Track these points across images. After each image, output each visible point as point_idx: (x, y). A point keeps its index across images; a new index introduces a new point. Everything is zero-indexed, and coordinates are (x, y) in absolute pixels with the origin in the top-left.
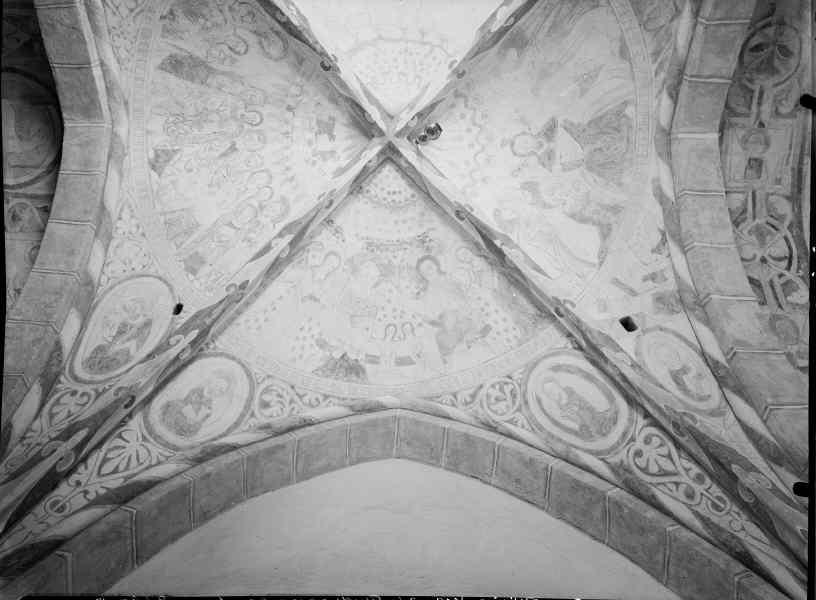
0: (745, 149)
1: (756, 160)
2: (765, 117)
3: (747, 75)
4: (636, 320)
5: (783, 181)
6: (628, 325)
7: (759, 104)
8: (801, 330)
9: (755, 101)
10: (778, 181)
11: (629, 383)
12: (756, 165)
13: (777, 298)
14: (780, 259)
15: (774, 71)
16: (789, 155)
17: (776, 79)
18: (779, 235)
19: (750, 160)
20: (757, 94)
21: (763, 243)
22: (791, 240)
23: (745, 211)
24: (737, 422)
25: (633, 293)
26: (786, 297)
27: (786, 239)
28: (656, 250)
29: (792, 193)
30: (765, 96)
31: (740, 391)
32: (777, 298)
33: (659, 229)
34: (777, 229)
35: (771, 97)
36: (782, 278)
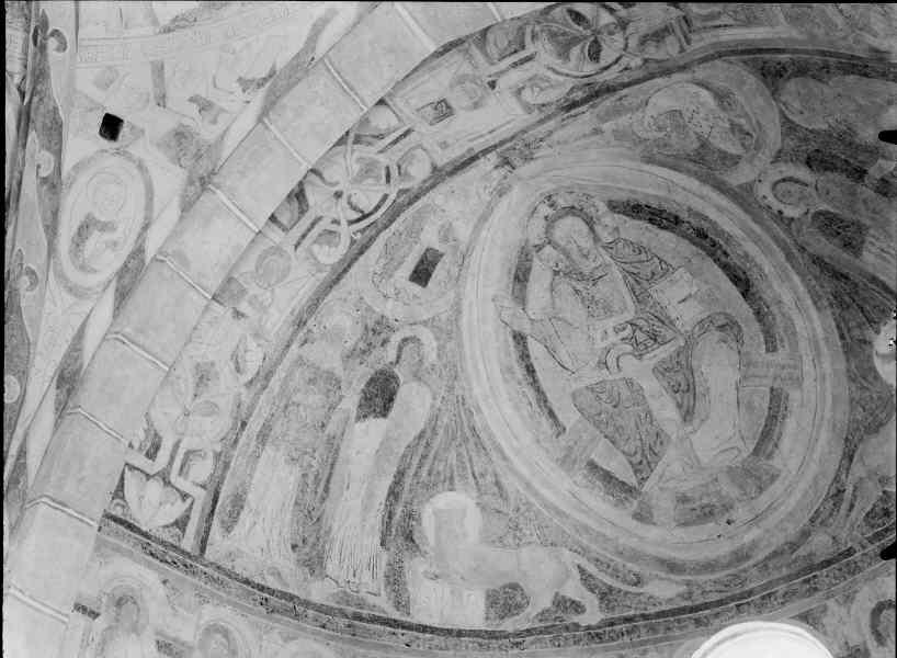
0: (451, 86)
1: (448, 107)
2: (502, 83)
3: (538, 28)
4: (124, 131)
5: (450, 149)
6: (111, 126)
7: (515, 65)
8: (288, 280)
9: (515, 58)
10: (444, 145)
11: (19, 190)
12: (443, 110)
13: (304, 236)
14: (355, 208)
15: (564, 53)
16: (482, 136)
17: (557, 63)
18: (384, 188)
19: (444, 101)
20: (522, 55)
21: (358, 180)
22: (389, 202)
23: (380, 137)
24: (84, 316)
25: (162, 100)
26: (315, 242)
27: (385, 197)
28: (245, 84)
29: (444, 167)
30: (527, 65)
31: (123, 295)
32: (304, 236)
33: (274, 66)
34: (388, 181)
35: (533, 72)
36: (335, 225)
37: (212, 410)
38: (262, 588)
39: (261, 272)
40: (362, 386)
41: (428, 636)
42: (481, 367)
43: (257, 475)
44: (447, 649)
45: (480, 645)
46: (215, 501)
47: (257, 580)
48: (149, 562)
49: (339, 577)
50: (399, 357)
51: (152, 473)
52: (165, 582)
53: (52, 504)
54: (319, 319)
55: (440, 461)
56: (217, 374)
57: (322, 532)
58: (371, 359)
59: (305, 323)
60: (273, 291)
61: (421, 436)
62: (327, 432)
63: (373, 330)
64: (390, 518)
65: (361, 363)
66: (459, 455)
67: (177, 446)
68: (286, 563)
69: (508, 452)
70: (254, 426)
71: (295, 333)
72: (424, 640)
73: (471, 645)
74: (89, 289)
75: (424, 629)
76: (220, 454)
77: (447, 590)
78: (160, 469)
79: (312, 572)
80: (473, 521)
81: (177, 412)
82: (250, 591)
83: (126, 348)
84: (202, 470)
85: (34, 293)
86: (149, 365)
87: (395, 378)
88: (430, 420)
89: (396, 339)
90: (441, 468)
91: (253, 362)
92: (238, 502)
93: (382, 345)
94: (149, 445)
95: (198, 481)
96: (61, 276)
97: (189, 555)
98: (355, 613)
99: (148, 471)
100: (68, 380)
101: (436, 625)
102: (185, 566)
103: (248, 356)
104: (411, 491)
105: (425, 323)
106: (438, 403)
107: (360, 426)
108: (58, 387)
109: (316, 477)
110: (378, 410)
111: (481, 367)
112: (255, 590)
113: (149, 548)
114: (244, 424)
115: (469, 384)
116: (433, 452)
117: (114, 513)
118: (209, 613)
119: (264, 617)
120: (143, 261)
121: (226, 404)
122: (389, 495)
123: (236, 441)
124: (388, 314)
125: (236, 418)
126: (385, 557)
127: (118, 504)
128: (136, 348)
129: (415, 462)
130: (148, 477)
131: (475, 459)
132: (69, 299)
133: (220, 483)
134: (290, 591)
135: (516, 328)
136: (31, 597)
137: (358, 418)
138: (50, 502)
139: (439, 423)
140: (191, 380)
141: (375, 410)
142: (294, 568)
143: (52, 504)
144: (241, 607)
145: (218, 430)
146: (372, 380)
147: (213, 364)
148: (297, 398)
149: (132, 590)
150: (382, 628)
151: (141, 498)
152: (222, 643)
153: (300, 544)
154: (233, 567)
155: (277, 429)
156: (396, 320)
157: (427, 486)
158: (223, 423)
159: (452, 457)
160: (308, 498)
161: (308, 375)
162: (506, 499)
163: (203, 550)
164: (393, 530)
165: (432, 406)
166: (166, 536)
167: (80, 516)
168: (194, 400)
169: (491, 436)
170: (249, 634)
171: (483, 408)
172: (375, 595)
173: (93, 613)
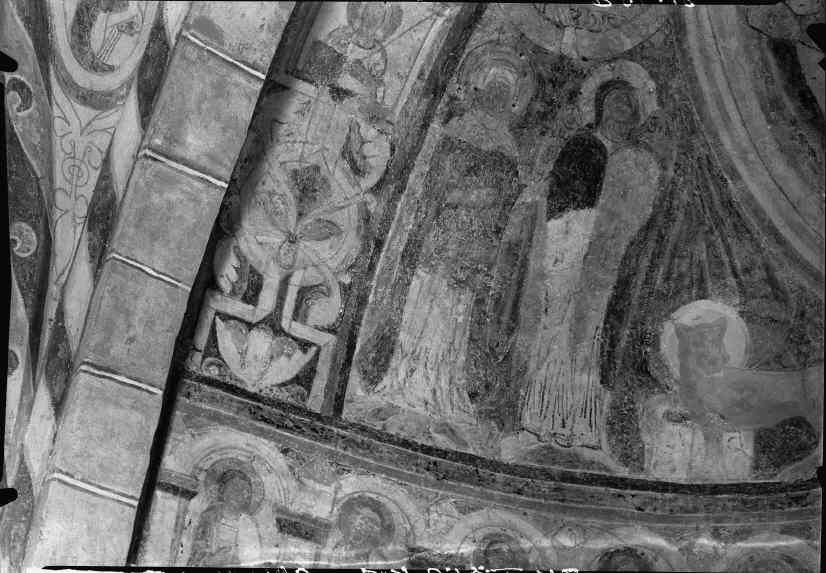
8: (399, 31)
31: (149, 95)
37: (329, 230)
38: (428, 450)
39: (357, 25)
40: (551, 166)
41: (669, 495)
42: (730, 107)
43: (408, 309)
44: (696, 510)
45: (744, 502)
46: (351, 347)
47: (420, 441)
48: (262, 429)
49: (540, 429)
50: (599, 114)
51: (254, 321)
52: (285, 452)
53: (96, 372)
54: (463, 79)
55: (681, 257)
56: (325, 180)
57: (513, 373)
58: (556, 125)
59: (444, 89)
60: (383, 50)
61: (649, 226)
62: (505, 239)
63: (551, 81)
64: (613, 345)
65: (543, 133)
66: (710, 245)
67: (285, 283)
68: (461, 415)
69: (786, 233)
70: (396, 243)
71: (432, 106)
72: (665, 501)
73: (730, 504)
74: (111, 94)
75: (663, 487)
76: (350, 286)
77: (700, 438)
78: (265, 314)
79: (502, 425)
80: (736, 338)
81: (276, 239)
82: (410, 455)
83: (160, 166)
84: (326, 310)
85: (31, 109)
86: (196, 184)
87: (601, 148)
88: (662, 200)
89: (590, 87)
90: (684, 269)
91: (378, 154)
92: (385, 346)
93: (570, 99)
94: (245, 286)
95: (319, 324)
96: (68, 84)
97: (319, 417)
98: (564, 473)
99: (249, 318)
100: (102, 218)
101: (683, 482)
102: (314, 430)
103: (368, 149)
104: (641, 305)
105: (630, 55)
106: (671, 173)
107: (555, 225)
108: (90, 230)
109: (497, 301)
110: (580, 198)
111: (730, 107)
112: (419, 454)
113: (260, 413)
114: (379, 244)
115: (716, 136)
116: (669, 247)
117: (206, 374)
118: (351, 484)
119: (433, 486)
120: (165, 43)
121: (348, 219)
122: (608, 315)
123: (372, 267)
124: (568, 50)
125: (365, 237)
126: (608, 397)
127: (212, 364)
128: (174, 165)
129: (645, 263)
130: (250, 326)
131: (735, 249)
132: (85, 113)
133: (357, 322)
134: (471, 451)
135: (775, 35)
136: (82, 480)
137: (551, 215)
138: (92, 370)
139: (676, 202)
140: (290, 197)
141: (574, 199)
142: (475, 422)
143: (96, 372)
144: (399, 475)
145: (343, 255)
146: (563, 154)
147: (317, 168)
148: (455, 196)
149: (240, 463)
150: (602, 489)
151: (243, 354)
152: (372, 520)
153: (482, 391)
154: (384, 427)
155: (431, 241)
156: (585, 59)
157: (663, 296)
158: (350, 245)
159: (701, 251)
160: (488, 330)
161: (464, 162)
162: (785, 301)
163: (338, 409)
164: (619, 362)
165: (662, 181)
166: (284, 396)
167: (136, 384)
168: (298, 220)
169: (757, 211)
170: (411, 507)
171: (741, 169)
172: (593, 448)
173: (188, 492)
